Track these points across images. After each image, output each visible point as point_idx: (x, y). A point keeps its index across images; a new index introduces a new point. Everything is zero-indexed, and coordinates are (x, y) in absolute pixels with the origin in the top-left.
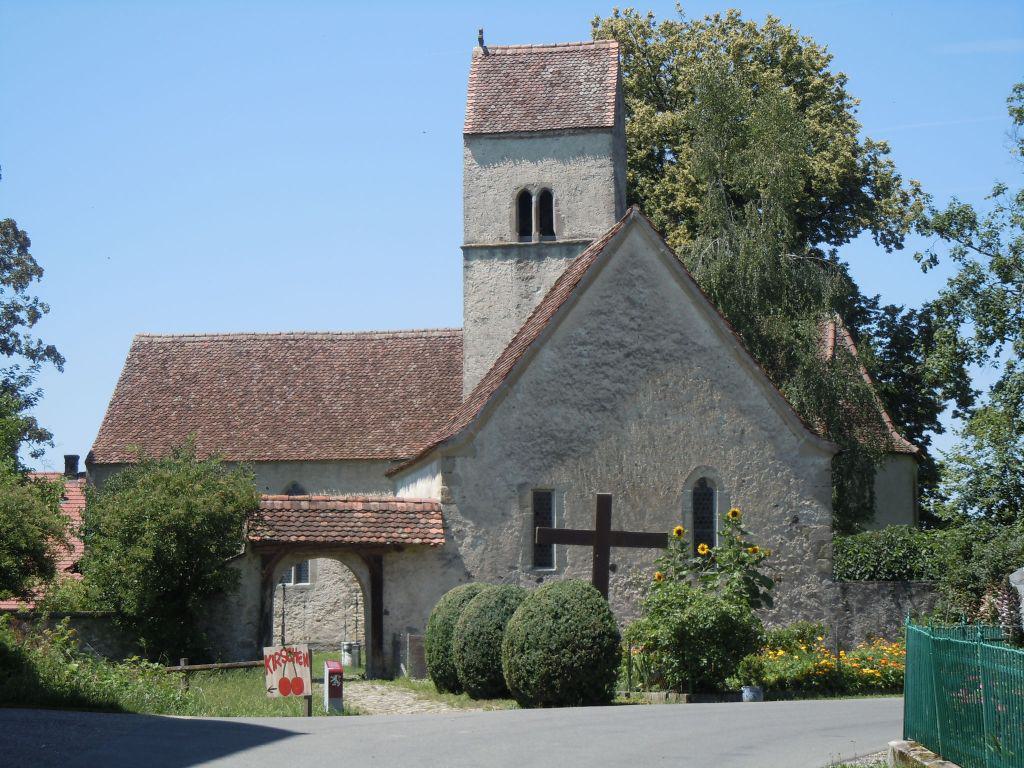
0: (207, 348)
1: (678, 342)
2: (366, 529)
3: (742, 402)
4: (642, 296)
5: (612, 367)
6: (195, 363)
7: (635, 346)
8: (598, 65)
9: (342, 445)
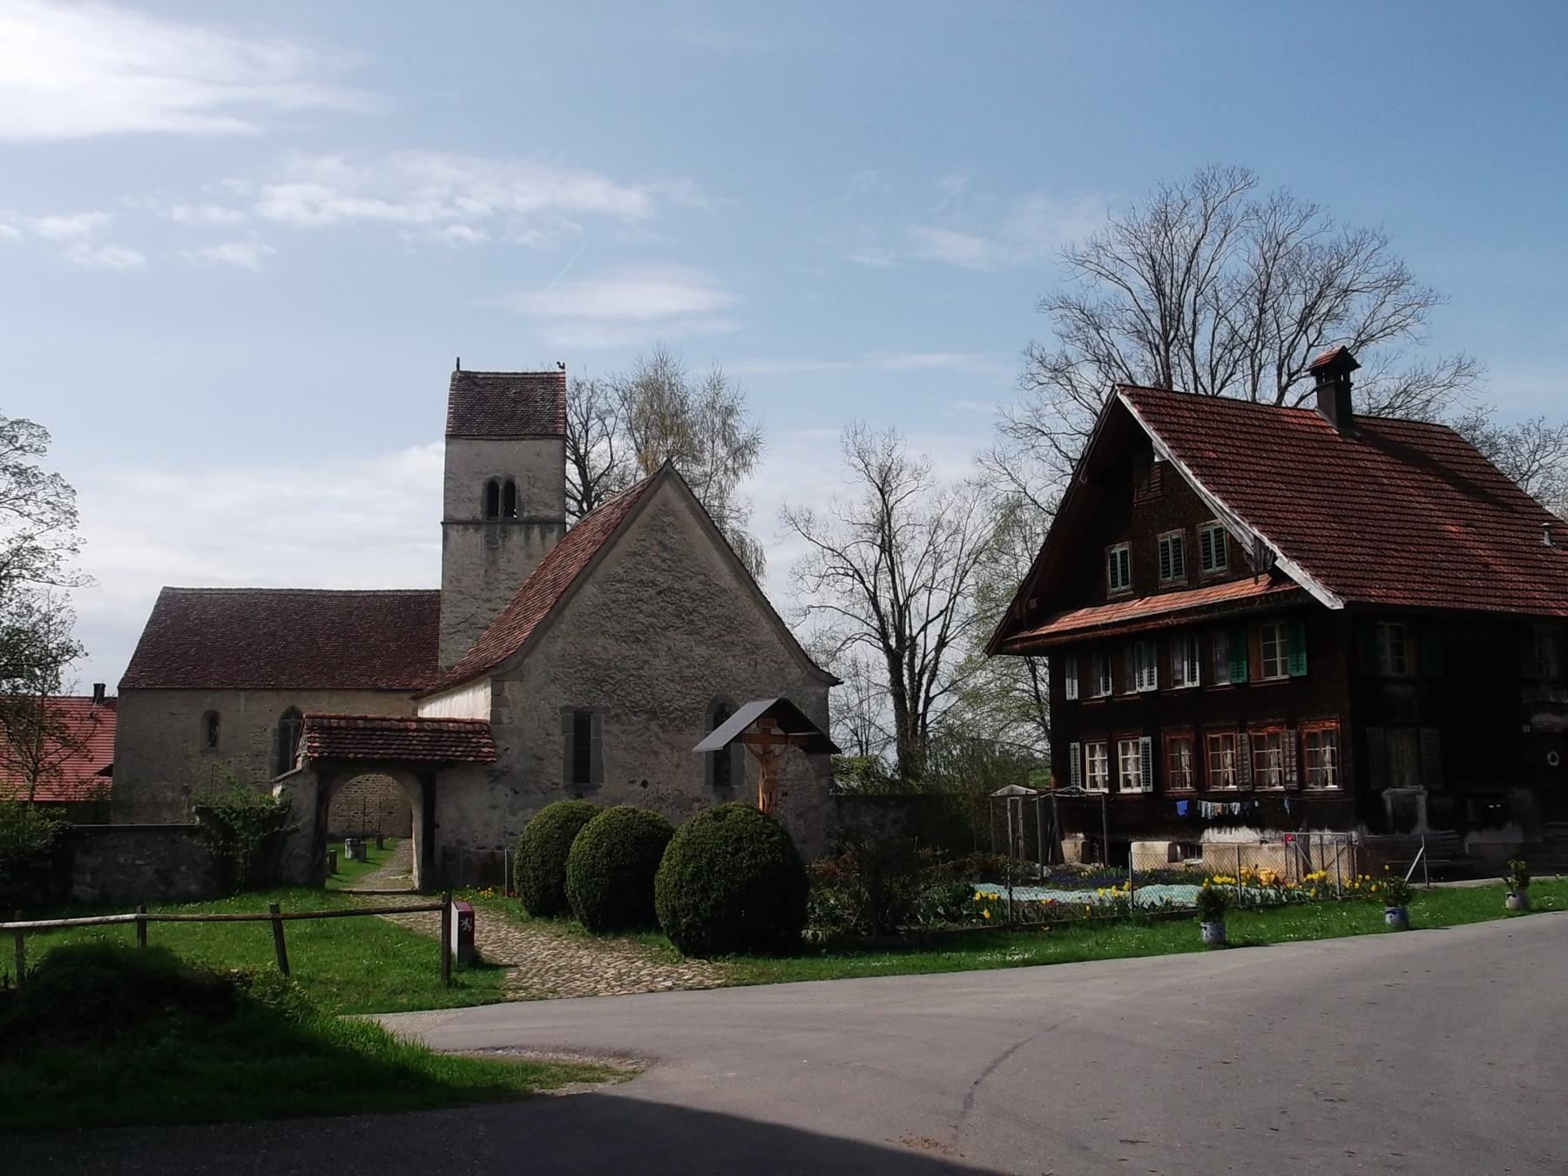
0: (222, 599)
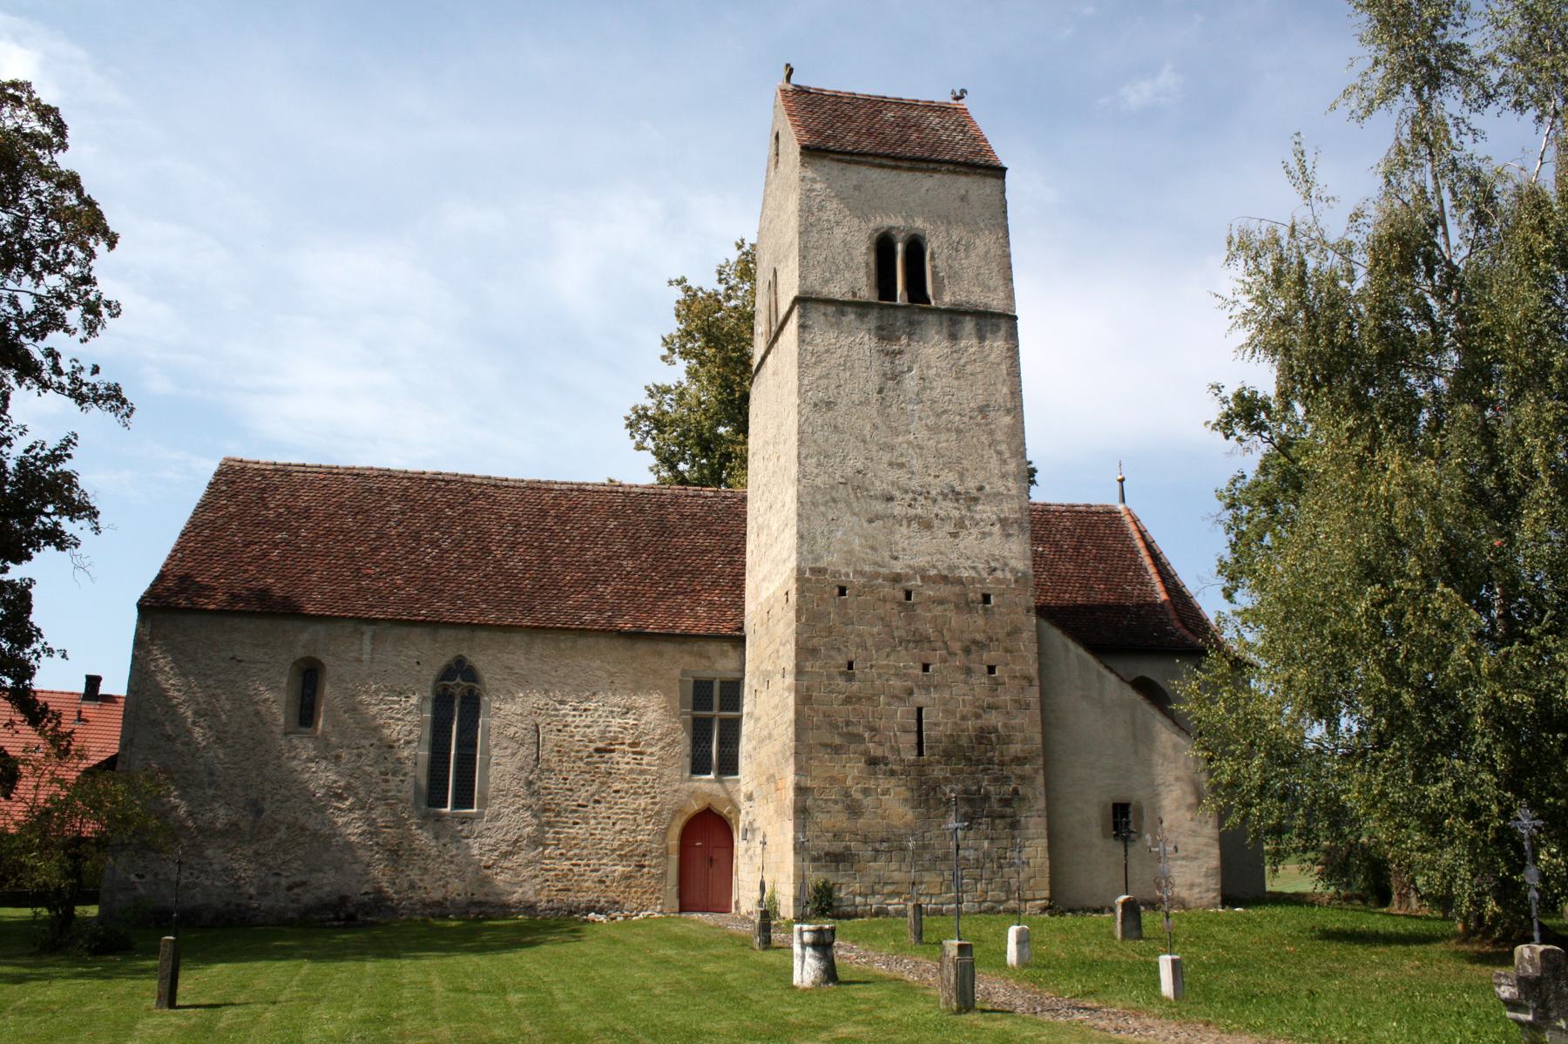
0: (323, 480)
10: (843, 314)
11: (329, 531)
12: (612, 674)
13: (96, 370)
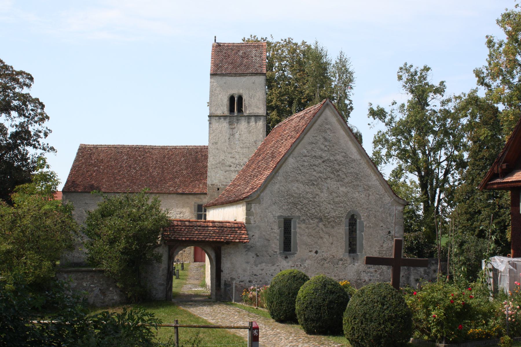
1: (344, 157)
2: (215, 235)
3: (369, 183)
4: (330, 136)
5: (317, 167)
6: (102, 155)
7: (326, 158)
8: (259, 51)
9: (157, 187)
10: (220, 119)
11: (108, 166)
12: (177, 204)
13: (48, 144)
